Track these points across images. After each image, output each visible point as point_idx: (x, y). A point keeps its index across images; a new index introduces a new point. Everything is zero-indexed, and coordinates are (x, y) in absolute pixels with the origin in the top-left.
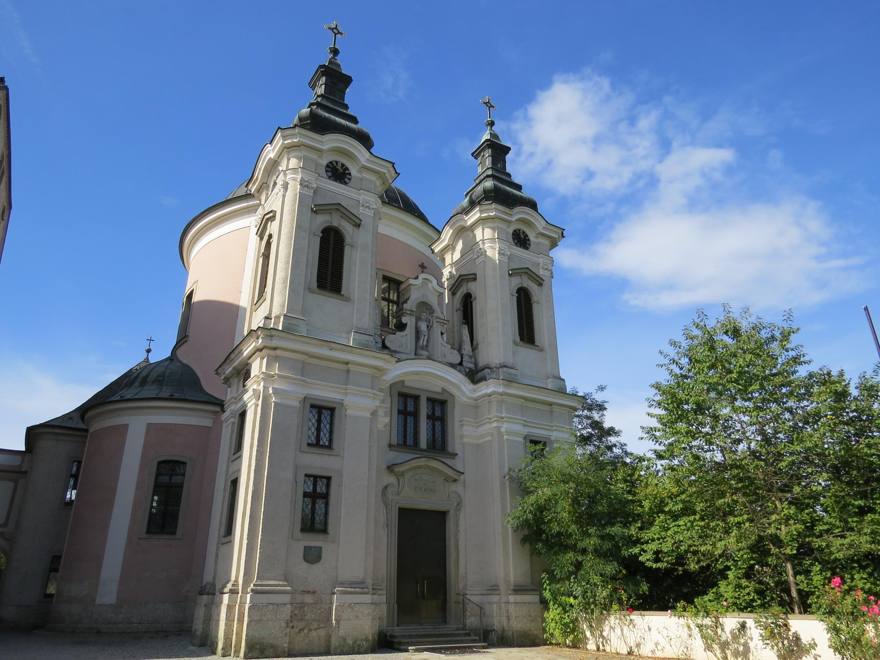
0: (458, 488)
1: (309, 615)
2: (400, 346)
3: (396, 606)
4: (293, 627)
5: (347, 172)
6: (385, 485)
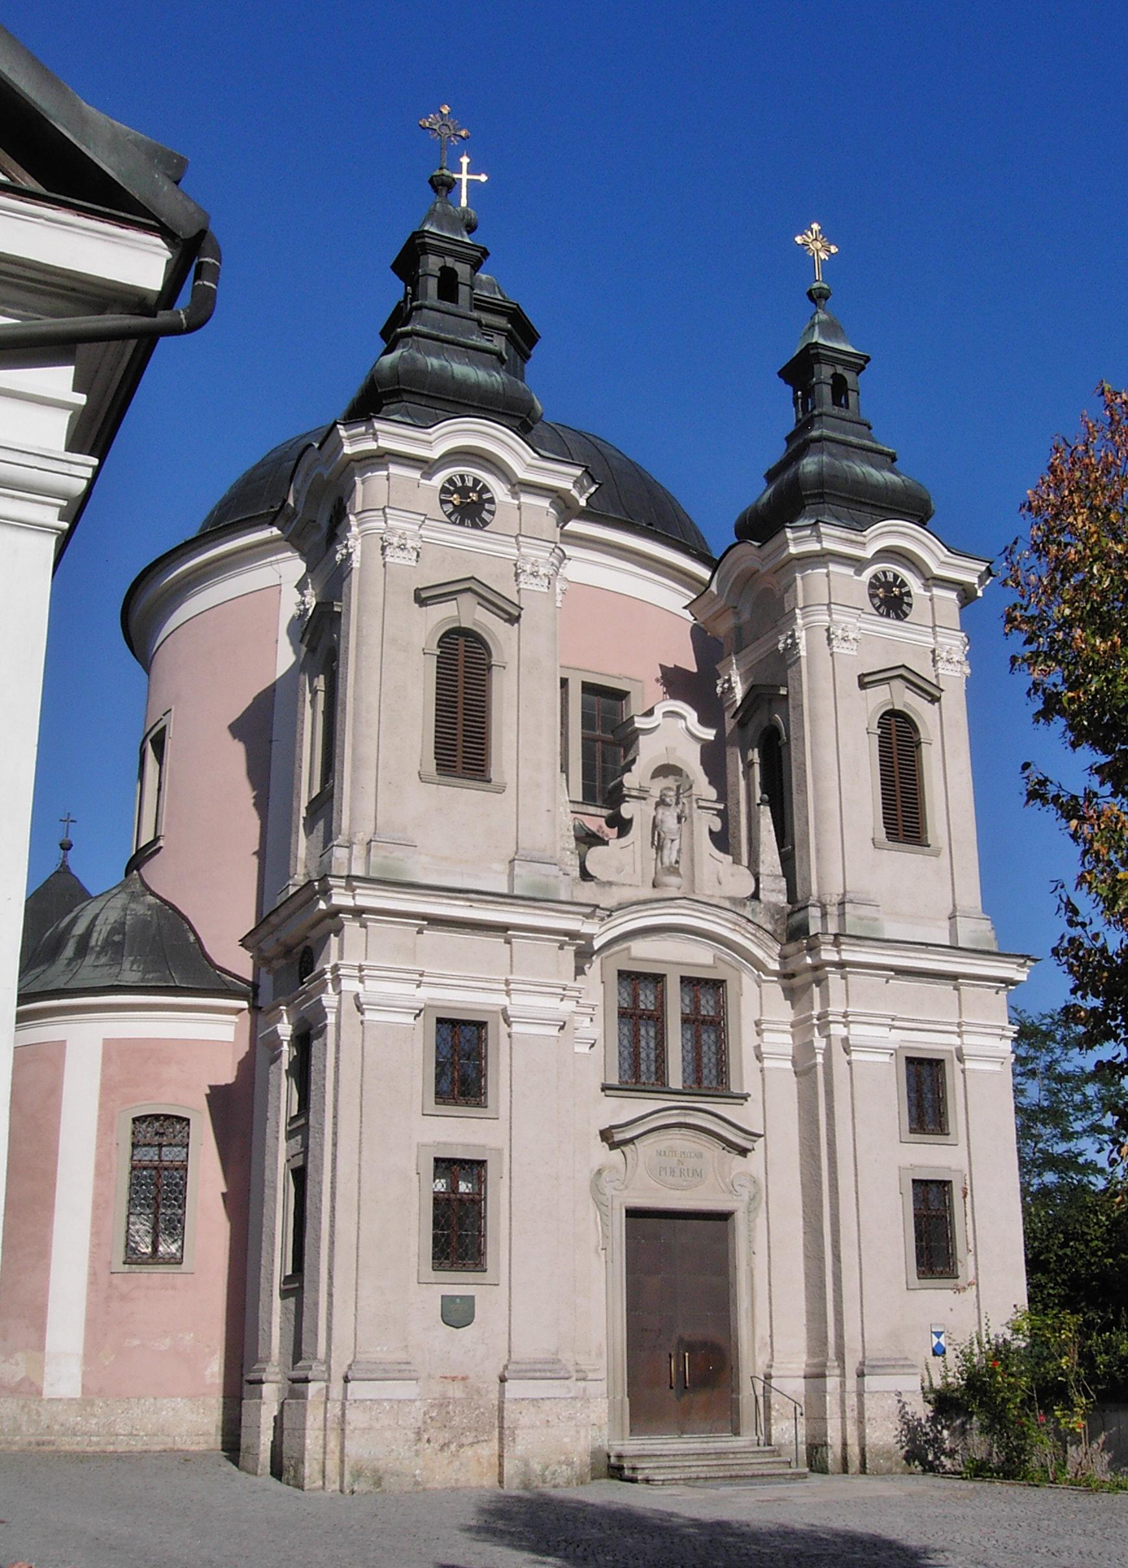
1: (457, 1419)
2: (619, 871)
3: (627, 1400)
4: (429, 1441)
5: (485, 496)
6: (596, 1169)
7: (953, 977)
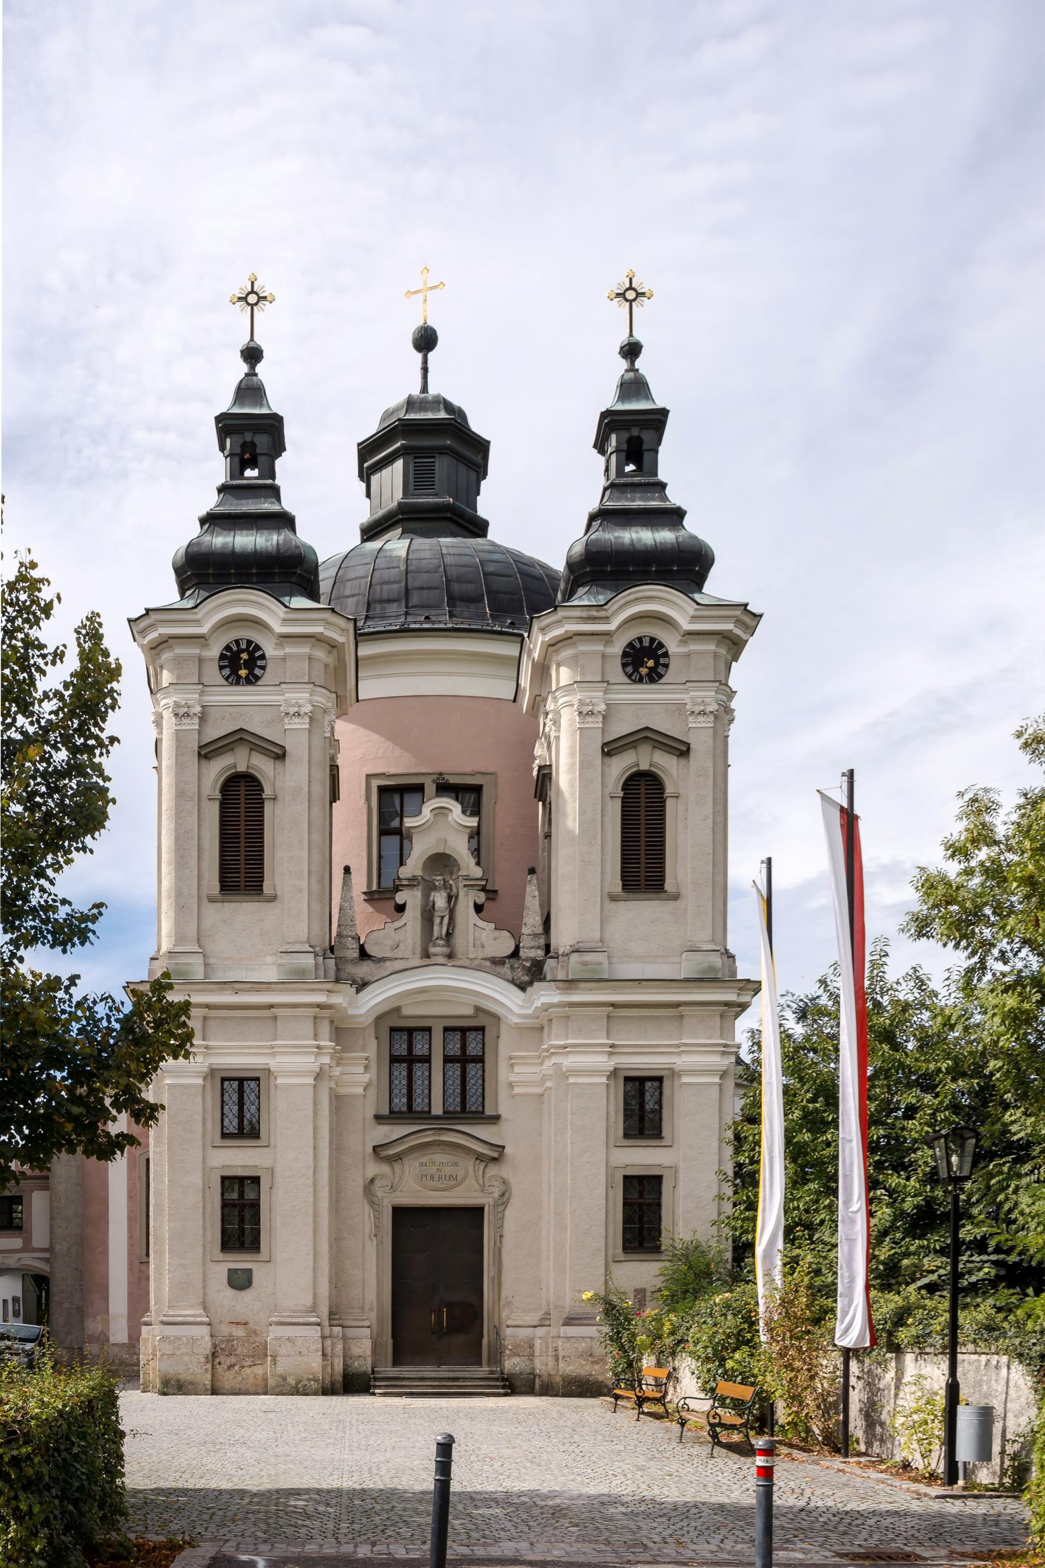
0: (504, 1171)
1: (239, 1349)
5: (257, 654)
7: (678, 1005)
